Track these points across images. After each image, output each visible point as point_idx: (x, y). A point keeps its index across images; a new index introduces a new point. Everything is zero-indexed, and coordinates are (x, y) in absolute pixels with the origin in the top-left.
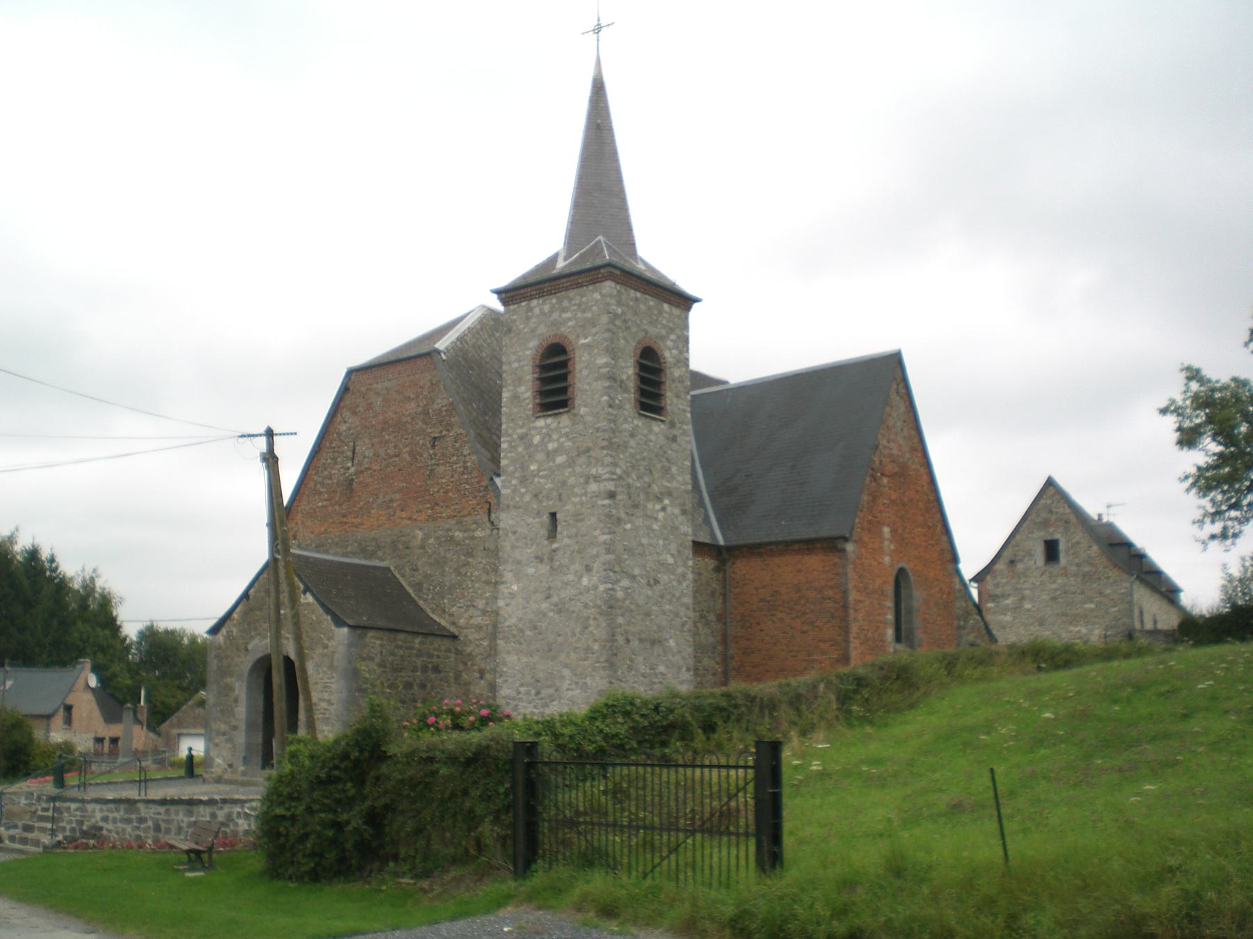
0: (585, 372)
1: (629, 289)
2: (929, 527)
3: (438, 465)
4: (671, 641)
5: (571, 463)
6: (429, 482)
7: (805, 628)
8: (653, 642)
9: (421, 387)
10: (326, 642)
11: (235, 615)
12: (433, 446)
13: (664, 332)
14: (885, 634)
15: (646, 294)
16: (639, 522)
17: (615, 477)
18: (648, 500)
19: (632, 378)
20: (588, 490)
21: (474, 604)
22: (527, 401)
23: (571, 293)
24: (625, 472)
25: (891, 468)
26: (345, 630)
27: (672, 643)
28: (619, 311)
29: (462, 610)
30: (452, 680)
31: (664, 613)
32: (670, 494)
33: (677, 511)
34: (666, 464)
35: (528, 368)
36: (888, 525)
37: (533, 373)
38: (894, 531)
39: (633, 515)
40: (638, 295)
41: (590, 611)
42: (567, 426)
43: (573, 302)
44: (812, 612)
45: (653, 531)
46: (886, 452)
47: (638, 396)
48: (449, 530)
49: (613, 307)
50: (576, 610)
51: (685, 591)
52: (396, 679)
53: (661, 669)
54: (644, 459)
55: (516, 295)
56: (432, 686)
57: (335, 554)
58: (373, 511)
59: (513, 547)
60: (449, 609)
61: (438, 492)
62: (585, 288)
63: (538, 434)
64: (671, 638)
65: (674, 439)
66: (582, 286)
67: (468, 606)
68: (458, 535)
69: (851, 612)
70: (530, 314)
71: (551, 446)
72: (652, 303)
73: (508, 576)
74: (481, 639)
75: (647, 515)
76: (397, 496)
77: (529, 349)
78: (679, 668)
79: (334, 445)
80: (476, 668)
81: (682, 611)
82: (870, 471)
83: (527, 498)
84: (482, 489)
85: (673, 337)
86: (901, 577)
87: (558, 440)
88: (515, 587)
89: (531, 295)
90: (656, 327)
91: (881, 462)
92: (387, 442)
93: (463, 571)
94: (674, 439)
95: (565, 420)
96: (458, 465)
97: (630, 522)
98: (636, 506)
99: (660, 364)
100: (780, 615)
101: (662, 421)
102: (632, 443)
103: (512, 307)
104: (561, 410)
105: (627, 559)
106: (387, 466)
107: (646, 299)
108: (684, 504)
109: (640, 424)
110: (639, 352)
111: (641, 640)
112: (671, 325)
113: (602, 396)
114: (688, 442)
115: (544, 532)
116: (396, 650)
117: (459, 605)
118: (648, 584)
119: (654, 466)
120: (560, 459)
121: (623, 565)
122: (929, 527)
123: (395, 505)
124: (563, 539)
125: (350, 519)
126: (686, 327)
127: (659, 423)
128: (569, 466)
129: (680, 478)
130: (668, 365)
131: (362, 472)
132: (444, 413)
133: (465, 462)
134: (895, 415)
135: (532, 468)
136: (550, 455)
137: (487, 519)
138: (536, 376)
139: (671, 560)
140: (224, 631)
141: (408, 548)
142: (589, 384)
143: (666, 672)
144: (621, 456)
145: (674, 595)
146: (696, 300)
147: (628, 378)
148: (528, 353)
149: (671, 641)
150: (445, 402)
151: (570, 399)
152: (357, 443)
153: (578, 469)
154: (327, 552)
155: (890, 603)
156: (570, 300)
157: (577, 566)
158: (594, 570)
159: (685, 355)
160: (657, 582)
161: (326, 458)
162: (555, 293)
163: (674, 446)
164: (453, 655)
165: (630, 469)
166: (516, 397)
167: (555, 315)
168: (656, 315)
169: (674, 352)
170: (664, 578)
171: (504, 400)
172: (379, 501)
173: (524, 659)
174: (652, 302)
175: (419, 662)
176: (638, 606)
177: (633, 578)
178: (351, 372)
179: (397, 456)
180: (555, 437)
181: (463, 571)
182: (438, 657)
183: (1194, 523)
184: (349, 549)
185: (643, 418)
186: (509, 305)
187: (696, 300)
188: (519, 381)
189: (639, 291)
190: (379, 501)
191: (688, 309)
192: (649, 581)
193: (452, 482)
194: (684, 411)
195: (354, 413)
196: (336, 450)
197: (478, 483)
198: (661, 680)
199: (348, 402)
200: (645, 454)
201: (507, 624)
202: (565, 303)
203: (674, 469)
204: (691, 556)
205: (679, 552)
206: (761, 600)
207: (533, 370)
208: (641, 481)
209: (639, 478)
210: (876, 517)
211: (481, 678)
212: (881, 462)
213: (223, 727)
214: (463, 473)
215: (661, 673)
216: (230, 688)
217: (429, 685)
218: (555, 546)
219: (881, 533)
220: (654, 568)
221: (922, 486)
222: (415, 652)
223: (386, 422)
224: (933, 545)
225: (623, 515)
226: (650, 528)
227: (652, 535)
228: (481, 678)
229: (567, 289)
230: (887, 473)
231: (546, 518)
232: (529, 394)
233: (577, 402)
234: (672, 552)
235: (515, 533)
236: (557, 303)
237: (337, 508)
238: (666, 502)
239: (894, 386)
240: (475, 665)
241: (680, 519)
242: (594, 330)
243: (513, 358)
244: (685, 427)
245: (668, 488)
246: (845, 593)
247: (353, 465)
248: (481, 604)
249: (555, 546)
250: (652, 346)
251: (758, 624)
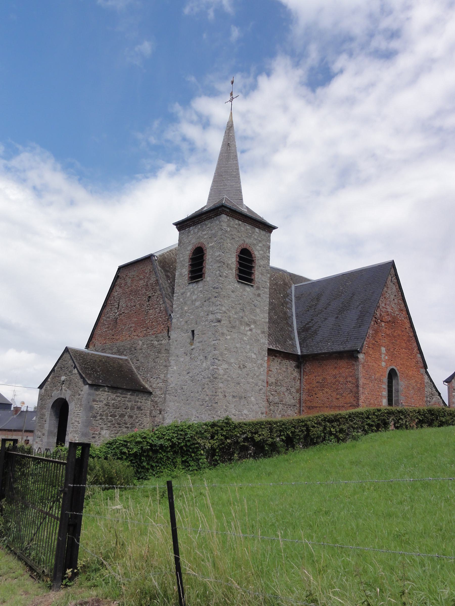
0: (210, 260)
1: (234, 219)
2: (409, 349)
3: (150, 309)
4: (252, 398)
5: (202, 306)
6: (146, 318)
7: (338, 397)
8: (241, 398)
9: (146, 273)
10: (80, 392)
11: (49, 380)
12: (149, 300)
13: (255, 242)
14: (381, 402)
15: (245, 222)
16: (235, 336)
17: (221, 312)
18: (241, 324)
19: (235, 263)
20: (209, 319)
21: (160, 377)
22: (186, 276)
23: (206, 222)
24: (227, 309)
25: (389, 318)
26: (87, 386)
27: (253, 399)
28: (229, 229)
29: (155, 379)
30: (148, 414)
31: (248, 383)
32: (255, 322)
33: (259, 332)
34: (253, 307)
35: (187, 260)
36: (384, 347)
37: (189, 262)
38: (388, 350)
39: (231, 331)
40: (240, 222)
41: (206, 380)
42: (201, 287)
43: (207, 226)
44: (341, 388)
45: (244, 341)
46: (384, 310)
47: (237, 272)
48: (152, 341)
49: (224, 227)
50: (200, 379)
51: (262, 373)
52: (115, 412)
53: (245, 412)
54: (240, 304)
56: (137, 417)
57: (109, 353)
58: (124, 332)
59: (175, 348)
60: (150, 379)
61: (149, 322)
62: (213, 219)
63: (189, 291)
64: (252, 396)
65: (259, 295)
66: (211, 218)
67: (157, 378)
68: (156, 343)
69: (360, 389)
70: (189, 234)
71: (194, 298)
72: (248, 227)
73: (173, 362)
74: (162, 394)
75: (240, 332)
76: (133, 325)
77: (188, 251)
78: (257, 413)
79: (111, 302)
80: (158, 408)
81: (260, 383)
82: (374, 319)
83: (183, 323)
84: (166, 320)
85: (260, 245)
86: (392, 374)
87: (197, 294)
88: (175, 368)
90: (250, 239)
91: (381, 315)
92: (131, 300)
93: (156, 360)
94: (259, 295)
95: (201, 284)
96: (158, 309)
97: (230, 335)
98: (234, 327)
99: (252, 257)
100: (326, 390)
101: (252, 286)
102: (233, 295)
103: (182, 231)
104: (199, 279)
105: (226, 354)
106: (130, 311)
107: (245, 225)
108: (264, 329)
109: (238, 287)
110: (239, 250)
111: (234, 397)
112: (260, 239)
113: (217, 271)
114: (266, 297)
115: (189, 341)
116: (116, 398)
117: (154, 377)
118: (240, 367)
119: (246, 308)
120: (197, 304)
121: (224, 356)
122: (409, 349)
123: (132, 329)
124: (196, 344)
125: (115, 337)
126: (269, 241)
127: (250, 287)
128: (201, 307)
129: (262, 315)
130: (257, 258)
131: (121, 314)
132: (154, 285)
133: (160, 308)
134: (390, 292)
135: (186, 308)
136: (193, 302)
137: (167, 335)
138: (190, 263)
139: (254, 356)
140: (44, 387)
141: (136, 350)
142: (212, 266)
143: (248, 414)
144: (226, 301)
145: (255, 374)
146: (274, 228)
147: (232, 263)
148: (187, 252)
149: (252, 398)
150: (155, 279)
151: (204, 273)
152: (120, 301)
153: (205, 309)
154: (105, 352)
155: (385, 386)
156: (207, 225)
157: (201, 357)
158: (209, 359)
159: (268, 254)
160: (245, 367)
161: (107, 309)
162: (200, 223)
163: (259, 298)
164: (150, 402)
165: (231, 308)
166: (181, 274)
167: (199, 234)
168: (250, 233)
169: (261, 252)
170: (249, 365)
171: (176, 276)
172: (126, 328)
173: (177, 404)
174: (248, 227)
175: (129, 404)
176: (232, 378)
177: (230, 364)
178: (121, 269)
179: (135, 306)
180: (196, 293)
181: (156, 360)
182: (141, 402)
184: (114, 351)
185: (240, 284)
186: (181, 230)
187: (274, 228)
188: (183, 265)
189: (240, 221)
190: (126, 328)
191: (271, 232)
192: (240, 366)
193: (155, 317)
194: (266, 282)
195: (120, 287)
196: (112, 304)
197: (165, 317)
198: (245, 417)
199: (118, 282)
200: (241, 301)
201: (171, 386)
202: (204, 227)
203: (258, 310)
204: (267, 355)
205: (259, 352)
206: (317, 383)
207: (189, 261)
208: (238, 315)
209: (236, 313)
210: (377, 342)
211: (160, 413)
212: (381, 315)
213: (40, 434)
214: (159, 313)
215: (245, 414)
216: (43, 415)
217: (135, 416)
218: (193, 347)
219: (380, 351)
220: (244, 359)
221: (406, 329)
222: (127, 399)
223: (132, 291)
224: (411, 359)
225: (225, 331)
226: (242, 339)
227: (243, 343)
228: (160, 413)
230: (384, 320)
231: (190, 334)
232: (187, 273)
233: (206, 275)
234: (255, 352)
235: (176, 341)
236: (201, 227)
237: (111, 331)
238: (253, 326)
239: (390, 278)
240: (158, 407)
241: (260, 335)
242: (215, 239)
243: (181, 255)
244: (266, 290)
245: (254, 319)
246: (357, 380)
247: (118, 311)
248: (162, 376)
249: (193, 347)
250: (248, 248)
251: (316, 394)
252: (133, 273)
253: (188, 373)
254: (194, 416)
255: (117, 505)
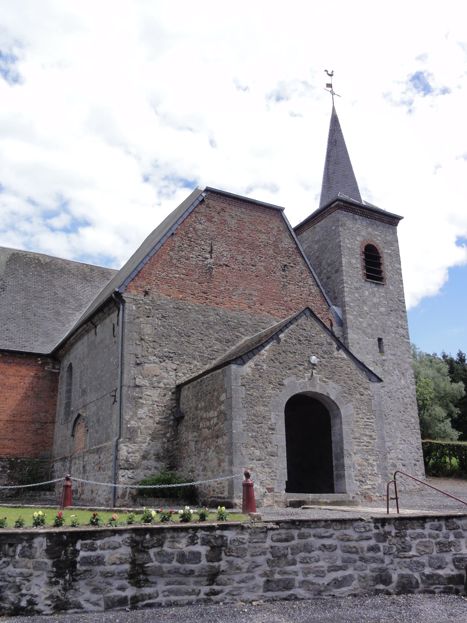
55: (349, 207)
62: (384, 224)
89: (357, 212)
95: (382, 290)
124: (388, 355)
146: (402, 218)
162: (369, 218)
183: (16, 80)
187: (402, 218)
229: (376, 219)
249: (384, 358)
252: (217, 204)
253: (383, 387)
254: (399, 439)
255: (280, 580)
